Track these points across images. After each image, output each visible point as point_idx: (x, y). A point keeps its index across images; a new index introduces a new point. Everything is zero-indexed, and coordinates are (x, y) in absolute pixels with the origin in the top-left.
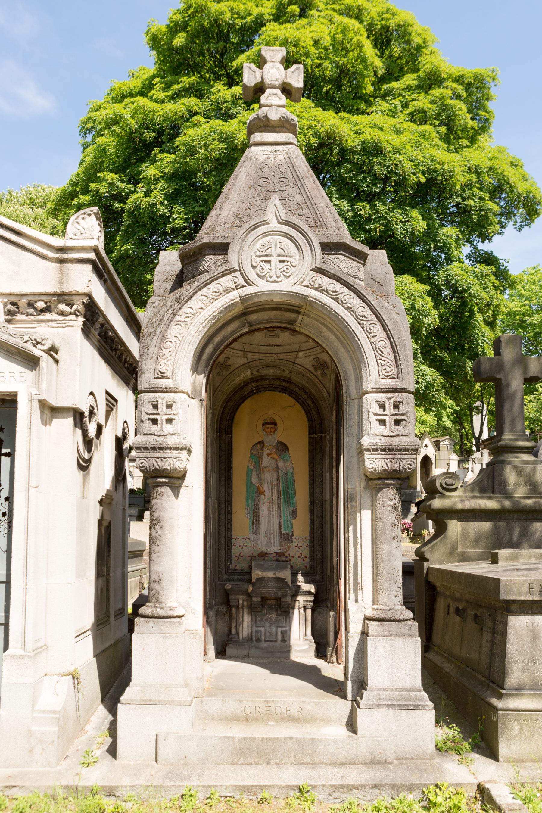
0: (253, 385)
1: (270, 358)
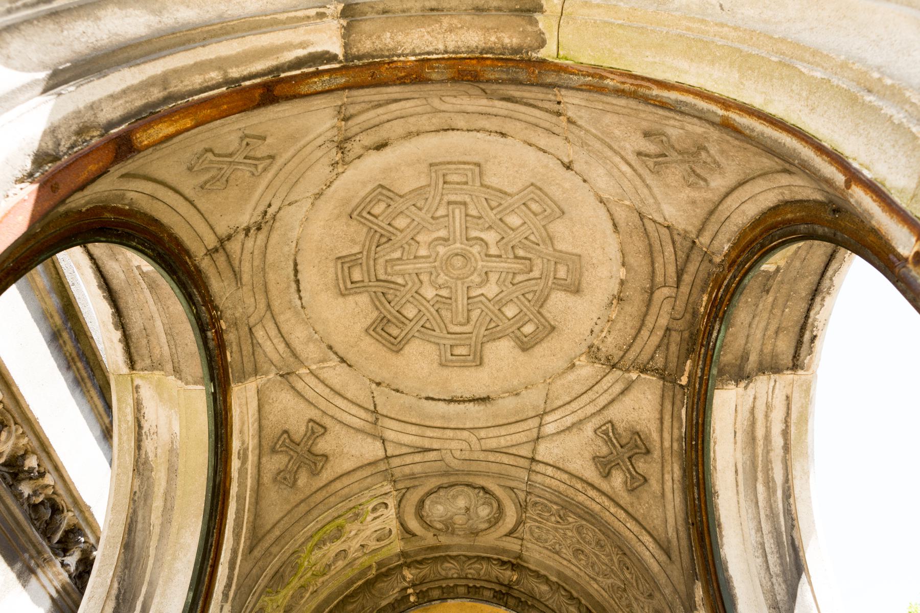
0: (408, 574)
1: (455, 448)
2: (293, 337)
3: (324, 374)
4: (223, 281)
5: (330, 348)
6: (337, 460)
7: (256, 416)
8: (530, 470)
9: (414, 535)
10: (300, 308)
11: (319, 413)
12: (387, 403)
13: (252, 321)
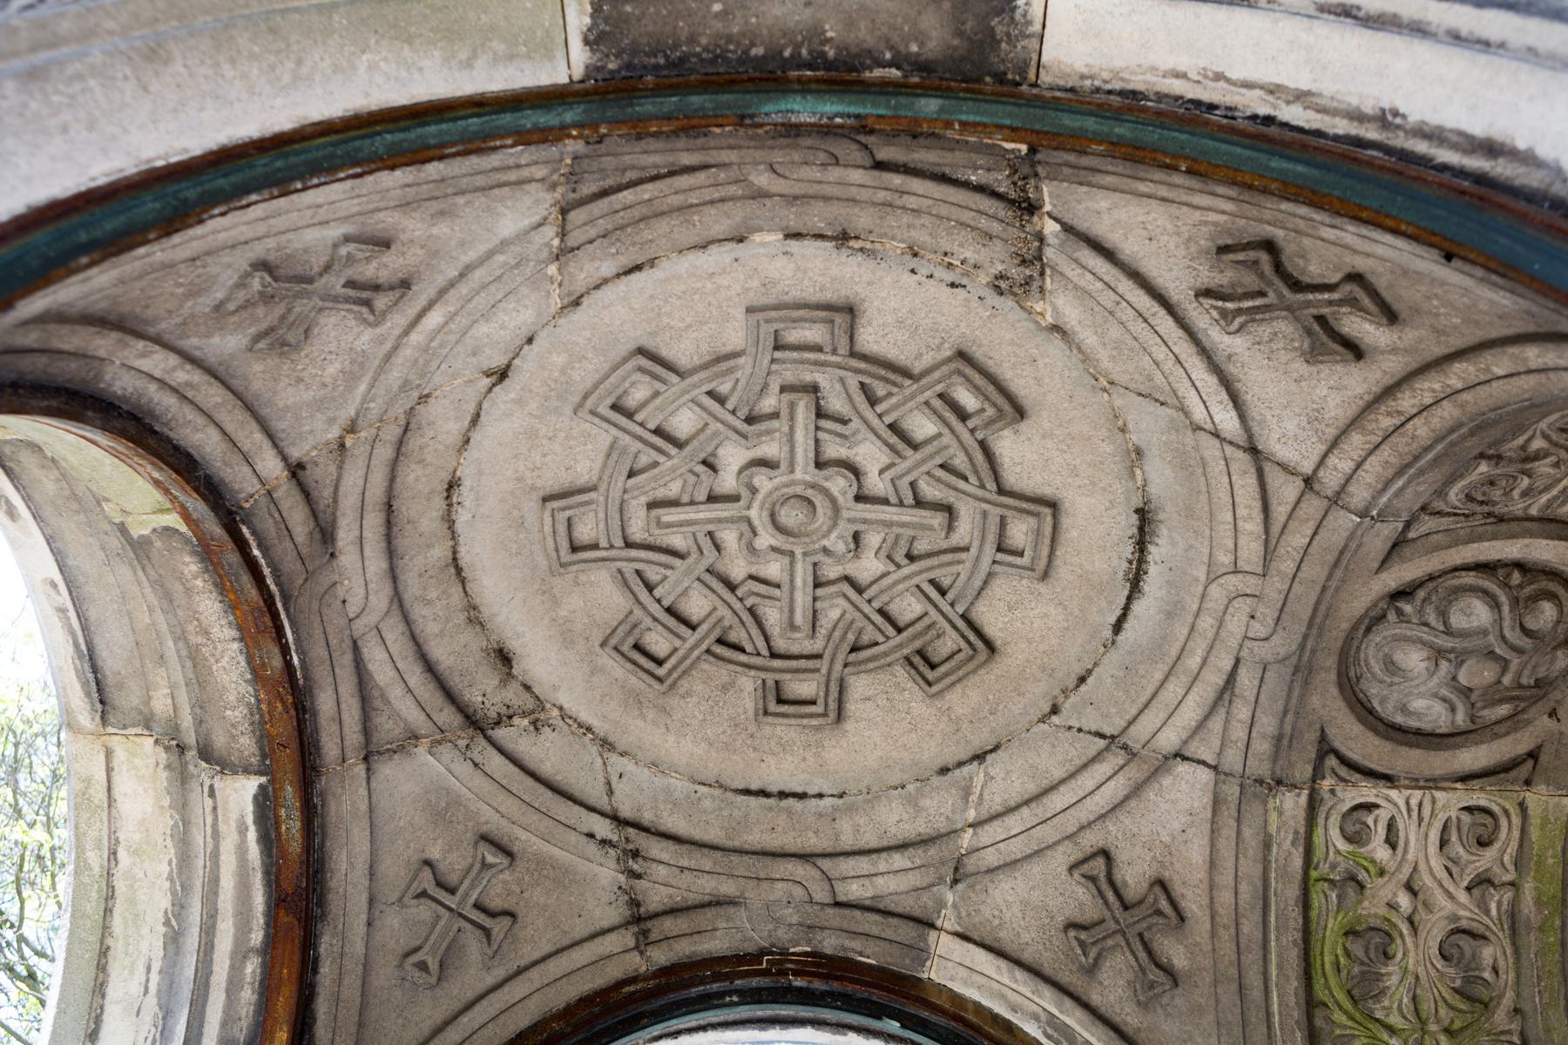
1: (1247, 627)
2: (893, 830)
3: (995, 802)
4: (715, 930)
5: (944, 771)
6: (1177, 866)
7: (1003, 964)
8: (1336, 500)
9: (1533, 755)
10: (840, 802)
11: (1067, 847)
12: (1100, 708)
13: (822, 895)
